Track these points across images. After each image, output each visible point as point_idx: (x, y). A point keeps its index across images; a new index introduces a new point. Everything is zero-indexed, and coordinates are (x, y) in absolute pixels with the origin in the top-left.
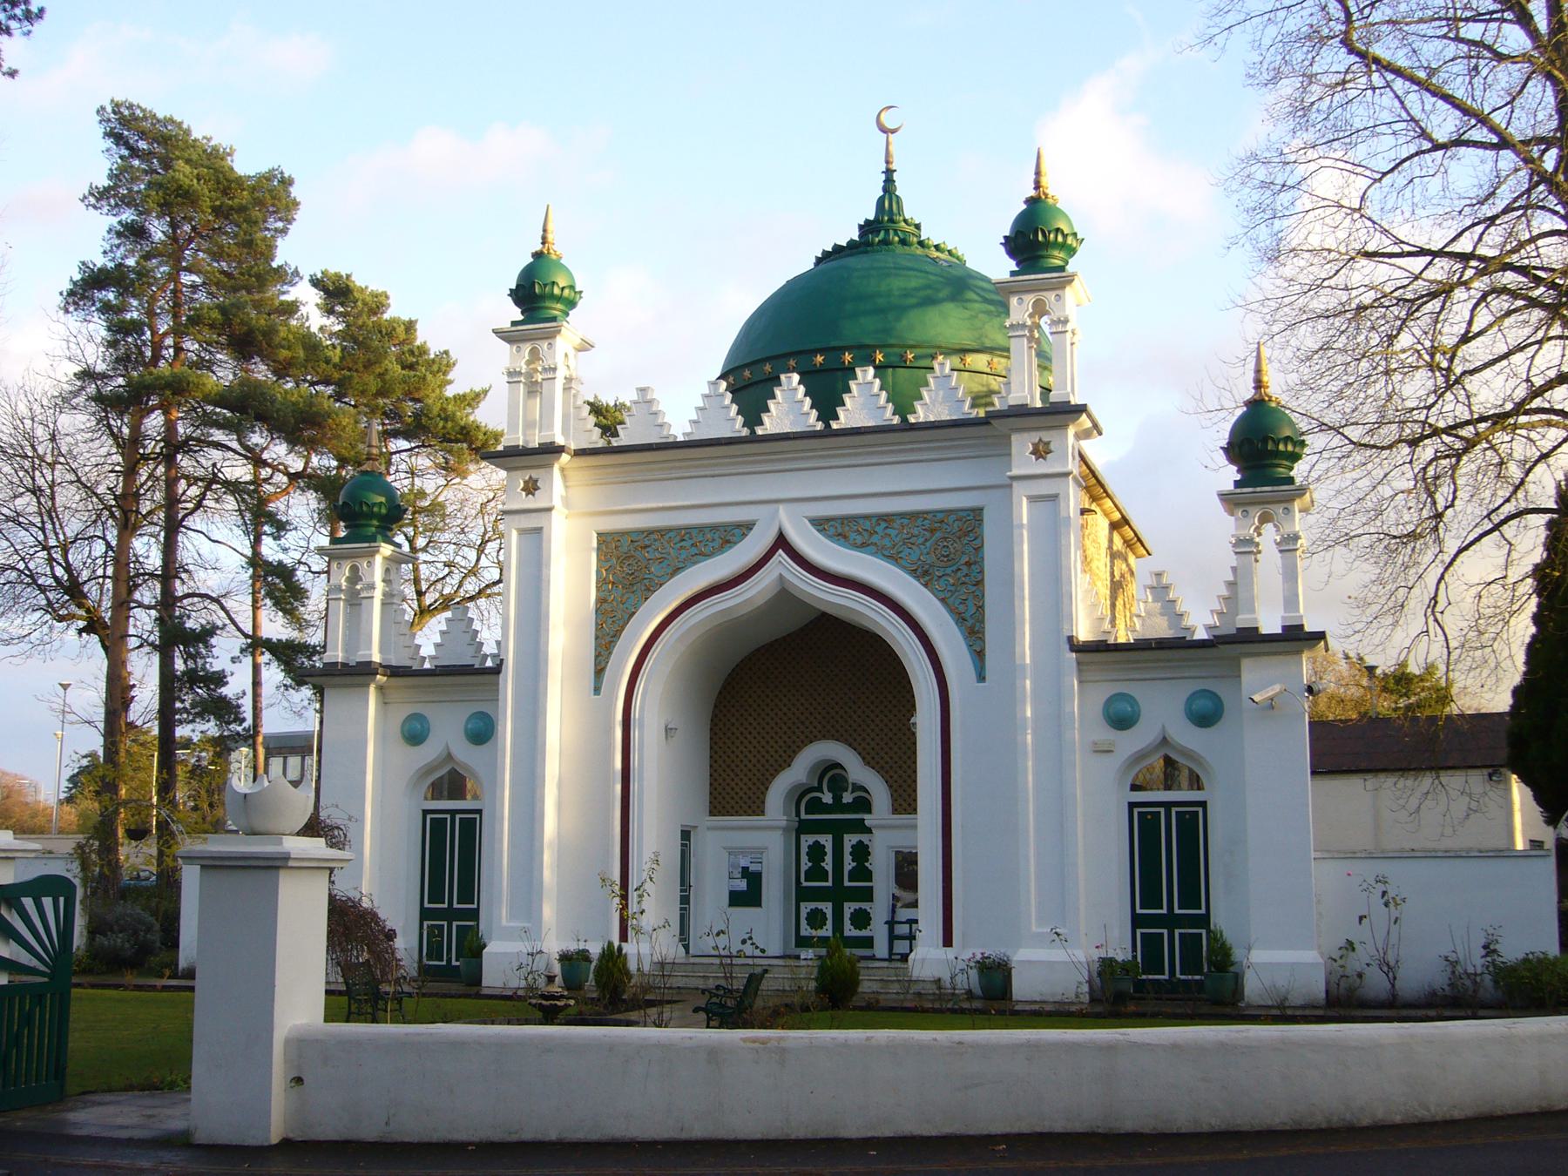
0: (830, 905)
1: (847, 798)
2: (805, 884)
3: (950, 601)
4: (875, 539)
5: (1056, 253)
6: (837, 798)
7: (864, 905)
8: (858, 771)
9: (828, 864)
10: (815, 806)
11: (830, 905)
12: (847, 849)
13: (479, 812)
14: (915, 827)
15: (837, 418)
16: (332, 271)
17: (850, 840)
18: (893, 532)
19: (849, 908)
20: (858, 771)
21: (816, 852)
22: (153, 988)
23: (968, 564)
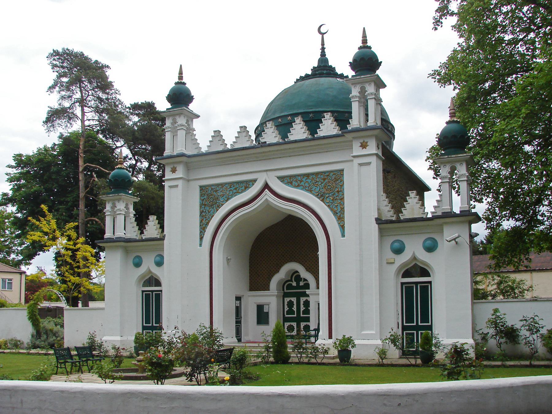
1: (302, 284)
2: (287, 316)
3: (331, 206)
4: (302, 183)
6: (298, 284)
7: (308, 323)
8: (304, 274)
9: (295, 308)
10: (290, 287)
12: (302, 303)
13: (161, 291)
14: (318, 294)
16: (147, 101)
17: (303, 299)
18: (309, 181)
19: (303, 325)
20: (304, 274)
21: (290, 304)
23: (338, 192)
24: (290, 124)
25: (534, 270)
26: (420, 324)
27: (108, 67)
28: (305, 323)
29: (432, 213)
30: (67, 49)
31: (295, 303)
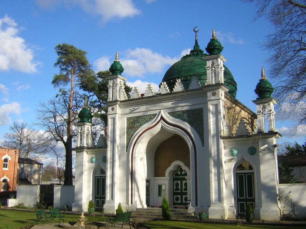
0: (180, 196)
1: (183, 173)
5: (216, 51)
6: (181, 173)
8: (184, 167)
9: (179, 187)
10: (177, 175)
11: (180, 196)
15: (173, 90)
19: (184, 197)
22: (95, 205)
24: (174, 84)
25: (301, 165)
26: (247, 198)
27: (86, 53)
28: (185, 196)
29: (235, 134)
30: (65, 44)
31: (180, 184)
